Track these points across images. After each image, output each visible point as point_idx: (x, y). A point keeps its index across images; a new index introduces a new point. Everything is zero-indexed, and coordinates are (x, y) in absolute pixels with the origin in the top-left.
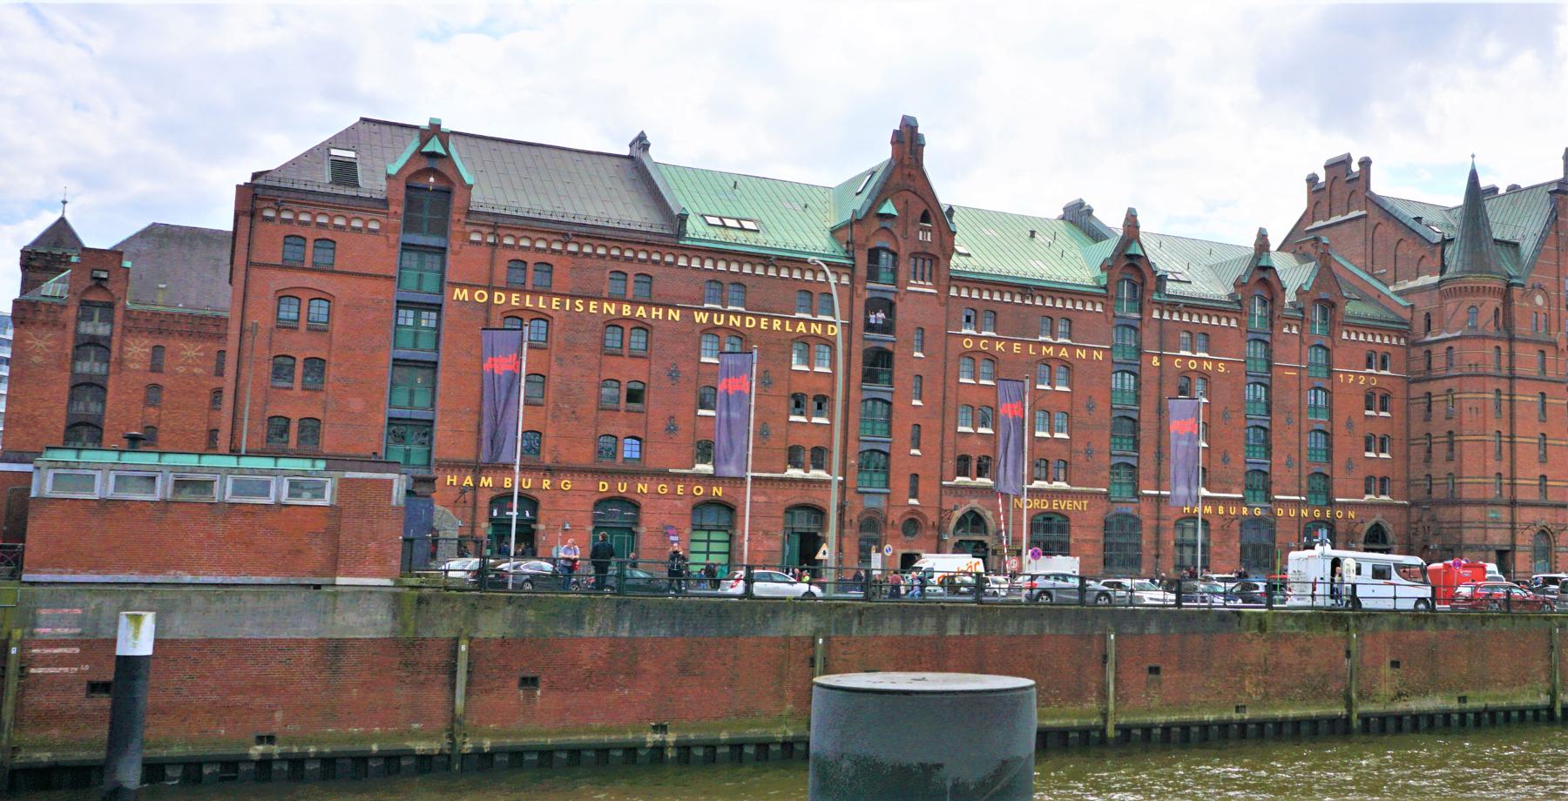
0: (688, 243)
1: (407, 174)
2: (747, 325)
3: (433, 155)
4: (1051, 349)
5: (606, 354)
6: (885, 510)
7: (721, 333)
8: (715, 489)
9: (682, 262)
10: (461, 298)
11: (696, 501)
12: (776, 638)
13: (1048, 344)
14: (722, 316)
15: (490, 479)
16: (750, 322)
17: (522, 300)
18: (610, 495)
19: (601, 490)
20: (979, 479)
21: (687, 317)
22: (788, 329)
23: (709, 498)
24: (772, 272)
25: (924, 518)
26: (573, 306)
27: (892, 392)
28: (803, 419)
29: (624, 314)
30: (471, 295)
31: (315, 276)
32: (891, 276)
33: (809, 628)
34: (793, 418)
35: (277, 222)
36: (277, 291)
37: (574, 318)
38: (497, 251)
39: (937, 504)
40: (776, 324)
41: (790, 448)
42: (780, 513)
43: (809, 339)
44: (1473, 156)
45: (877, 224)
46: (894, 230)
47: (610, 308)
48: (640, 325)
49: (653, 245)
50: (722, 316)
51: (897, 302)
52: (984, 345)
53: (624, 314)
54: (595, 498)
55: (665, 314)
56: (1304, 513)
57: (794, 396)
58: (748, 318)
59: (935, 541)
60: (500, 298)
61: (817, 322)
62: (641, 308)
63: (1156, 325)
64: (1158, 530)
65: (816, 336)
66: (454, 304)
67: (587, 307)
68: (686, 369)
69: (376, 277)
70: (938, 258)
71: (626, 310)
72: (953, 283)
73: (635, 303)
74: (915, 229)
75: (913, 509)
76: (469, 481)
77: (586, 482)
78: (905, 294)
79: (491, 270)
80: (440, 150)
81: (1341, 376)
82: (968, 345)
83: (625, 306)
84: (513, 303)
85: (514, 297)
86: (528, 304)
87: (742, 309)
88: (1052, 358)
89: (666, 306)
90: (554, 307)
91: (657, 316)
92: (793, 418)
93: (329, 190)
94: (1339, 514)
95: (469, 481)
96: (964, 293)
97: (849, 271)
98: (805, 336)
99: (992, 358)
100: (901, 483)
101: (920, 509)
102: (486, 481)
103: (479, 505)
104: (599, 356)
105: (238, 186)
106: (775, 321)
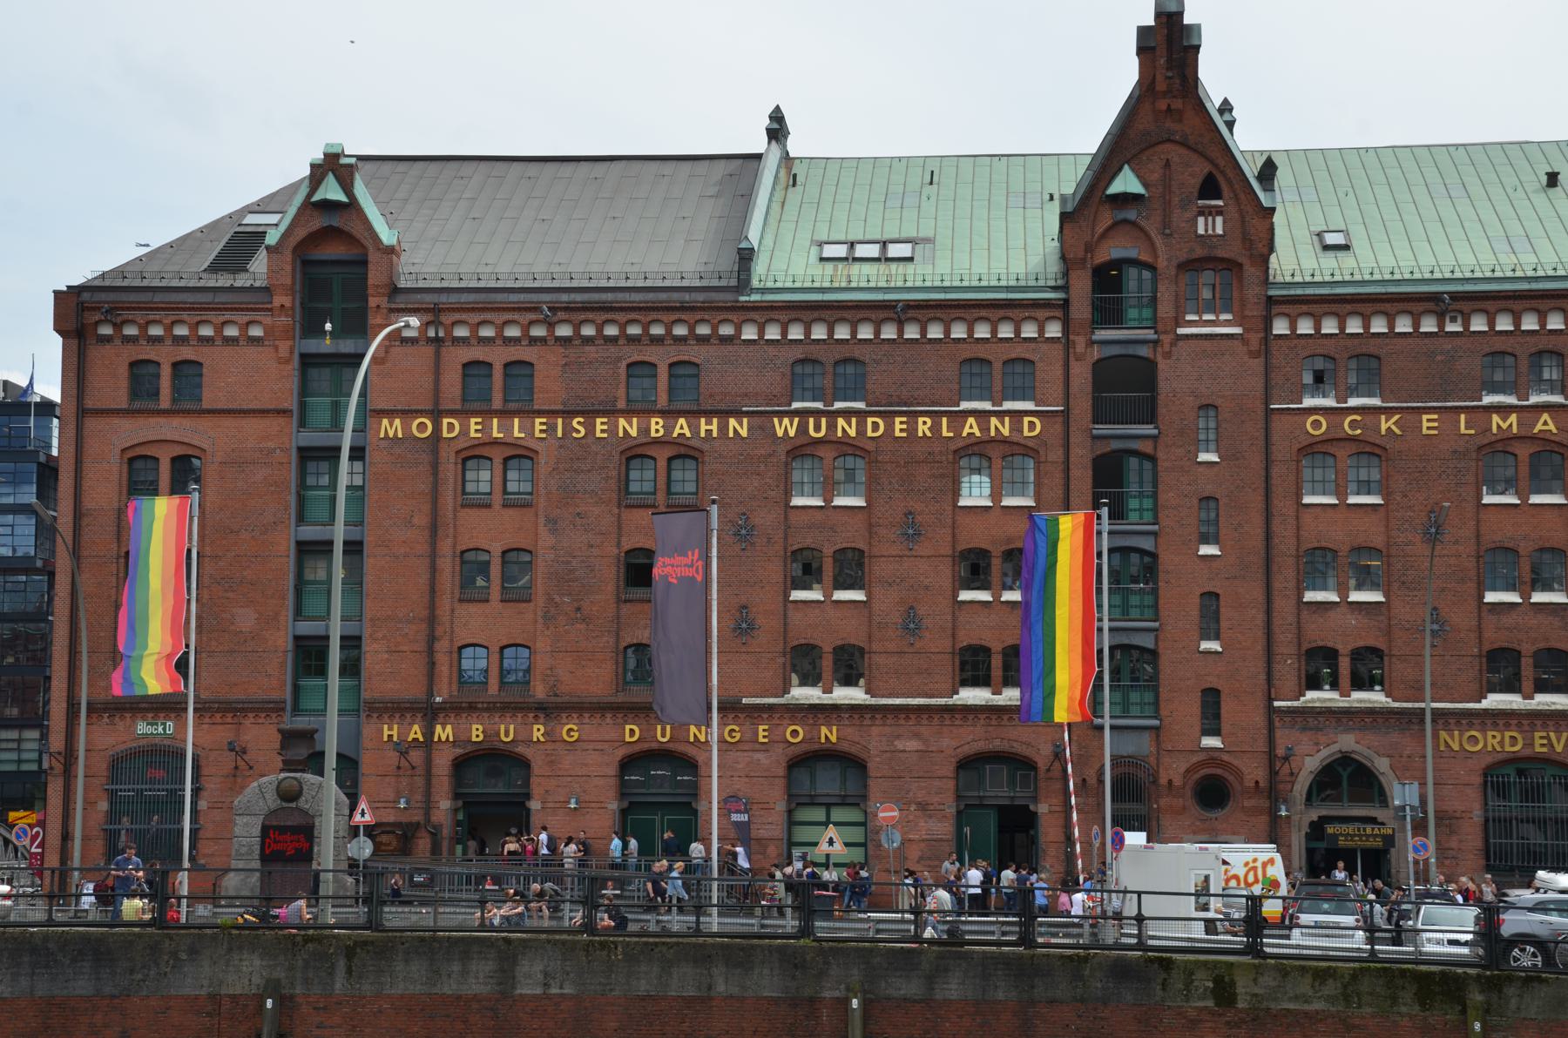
0: (755, 297)
1: (294, 241)
2: (870, 434)
3: (328, 206)
4: (1513, 418)
5: (628, 506)
6: (1152, 760)
7: (827, 453)
8: (824, 730)
9: (749, 333)
10: (391, 434)
11: (791, 751)
12: (197, 997)
13: (1504, 410)
14: (824, 420)
15: (449, 728)
16: (875, 427)
17: (485, 429)
18: (646, 746)
19: (628, 739)
20: (1357, 695)
21: (761, 428)
22: (945, 433)
23: (816, 747)
24: (912, 332)
25: (1239, 774)
26: (568, 429)
27: (1155, 534)
28: (984, 596)
29: (653, 434)
30: (406, 427)
31: (176, 421)
32: (1147, 313)
33: (256, 980)
34: (965, 596)
35: (118, 342)
36: (123, 451)
37: (576, 454)
38: (444, 350)
39: (1262, 745)
40: (924, 426)
41: (964, 650)
42: (948, 769)
43: (989, 446)
45: (1106, 218)
46: (1143, 223)
47: (629, 427)
48: (683, 451)
49: (693, 309)
50: (824, 420)
51: (1159, 359)
52: (1353, 424)
53: (653, 434)
54: (621, 753)
55: (723, 428)
57: (966, 554)
58: (870, 420)
59: (1264, 819)
60: (451, 427)
61: (1000, 415)
62: (682, 421)
65: (1001, 441)
66: (384, 444)
67: (590, 429)
68: (766, 518)
69: (263, 412)
70: (1240, 265)
71: (657, 426)
72: (1276, 309)
73: (670, 414)
74: (1188, 215)
75: (1212, 754)
76: (416, 732)
77: (604, 728)
78: (1173, 344)
79: (437, 381)
80: (337, 195)
82: (1316, 428)
83: (653, 420)
84: (473, 434)
85: (474, 424)
86: (495, 434)
87: (861, 405)
89: (724, 414)
90: (537, 434)
91: (709, 432)
92: (965, 596)
93: (202, 283)
95: (416, 732)
96: (1305, 327)
97: (1059, 313)
98: (980, 442)
99: (1370, 449)
100: (1184, 710)
101: (1226, 757)
102: (444, 732)
103: (434, 771)
104: (616, 511)
105: (57, 293)
106: (921, 420)
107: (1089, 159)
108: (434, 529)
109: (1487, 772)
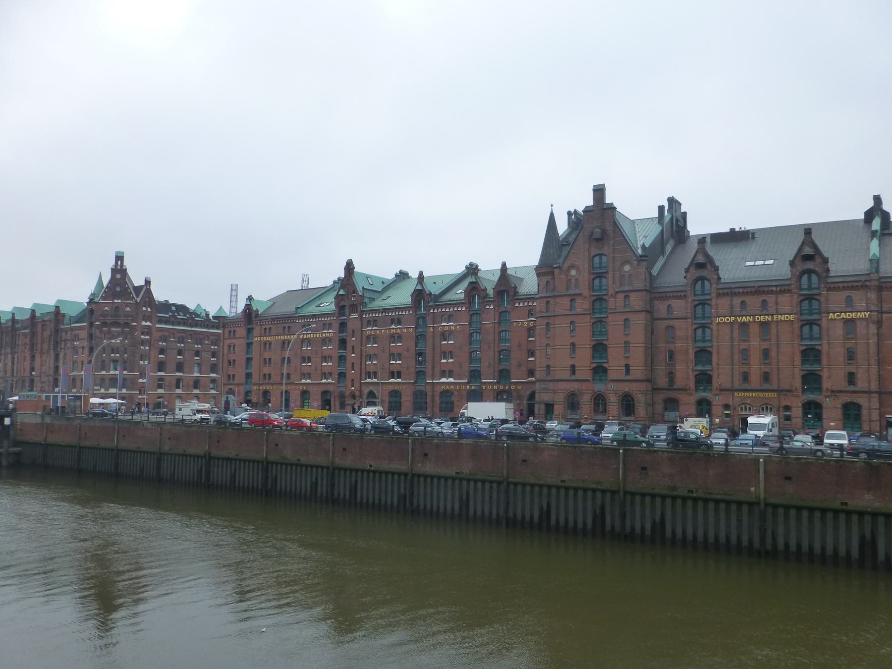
2: (756, 320)
13: (393, 329)
44: (552, 206)
56: (496, 387)
63: (432, 314)
64: (433, 396)
76: (258, 388)
81: (515, 324)
87: (310, 332)
88: (395, 334)
94: (513, 387)
100: (349, 383)
102: (261, 388)
107: (657, 219)
108: (260, 355)
109: (390, 393)
